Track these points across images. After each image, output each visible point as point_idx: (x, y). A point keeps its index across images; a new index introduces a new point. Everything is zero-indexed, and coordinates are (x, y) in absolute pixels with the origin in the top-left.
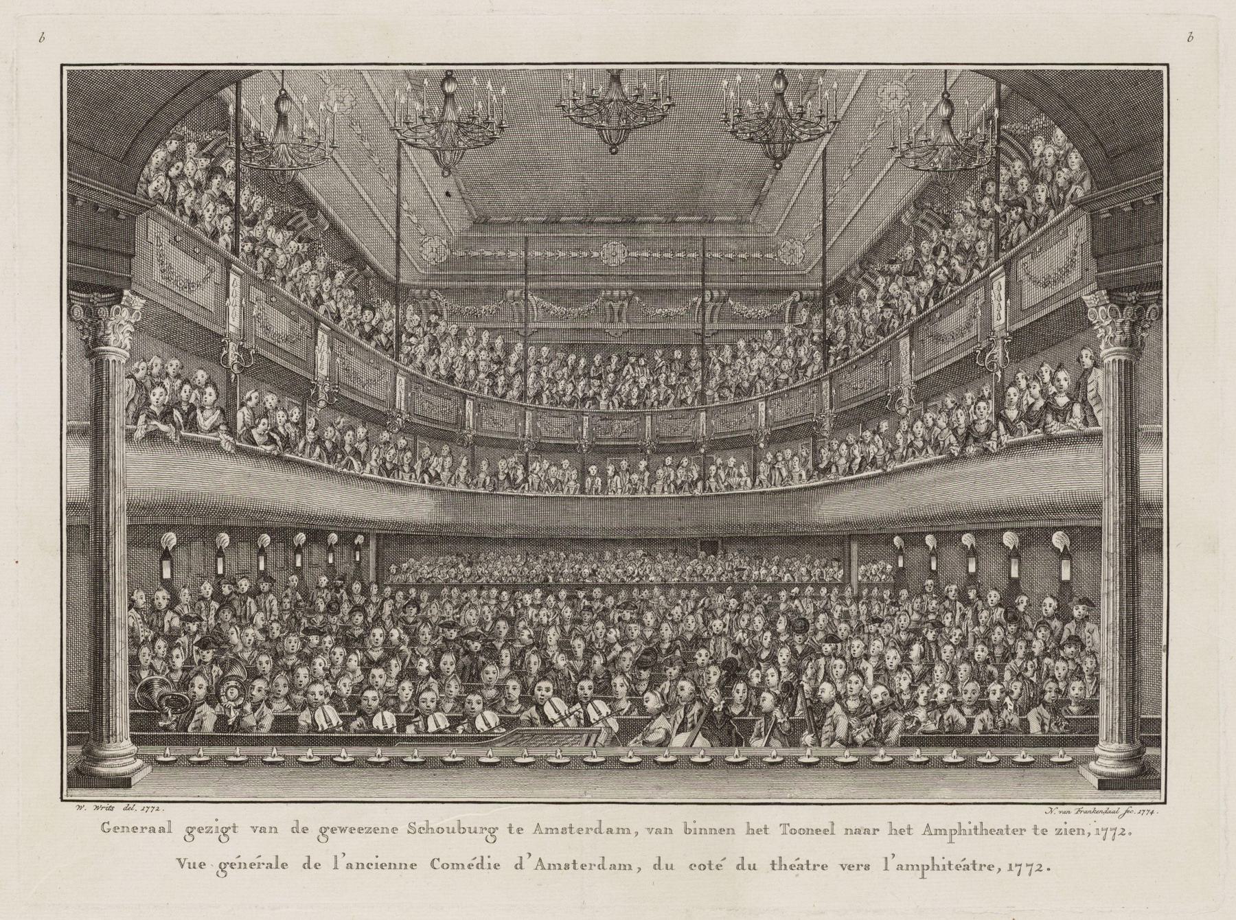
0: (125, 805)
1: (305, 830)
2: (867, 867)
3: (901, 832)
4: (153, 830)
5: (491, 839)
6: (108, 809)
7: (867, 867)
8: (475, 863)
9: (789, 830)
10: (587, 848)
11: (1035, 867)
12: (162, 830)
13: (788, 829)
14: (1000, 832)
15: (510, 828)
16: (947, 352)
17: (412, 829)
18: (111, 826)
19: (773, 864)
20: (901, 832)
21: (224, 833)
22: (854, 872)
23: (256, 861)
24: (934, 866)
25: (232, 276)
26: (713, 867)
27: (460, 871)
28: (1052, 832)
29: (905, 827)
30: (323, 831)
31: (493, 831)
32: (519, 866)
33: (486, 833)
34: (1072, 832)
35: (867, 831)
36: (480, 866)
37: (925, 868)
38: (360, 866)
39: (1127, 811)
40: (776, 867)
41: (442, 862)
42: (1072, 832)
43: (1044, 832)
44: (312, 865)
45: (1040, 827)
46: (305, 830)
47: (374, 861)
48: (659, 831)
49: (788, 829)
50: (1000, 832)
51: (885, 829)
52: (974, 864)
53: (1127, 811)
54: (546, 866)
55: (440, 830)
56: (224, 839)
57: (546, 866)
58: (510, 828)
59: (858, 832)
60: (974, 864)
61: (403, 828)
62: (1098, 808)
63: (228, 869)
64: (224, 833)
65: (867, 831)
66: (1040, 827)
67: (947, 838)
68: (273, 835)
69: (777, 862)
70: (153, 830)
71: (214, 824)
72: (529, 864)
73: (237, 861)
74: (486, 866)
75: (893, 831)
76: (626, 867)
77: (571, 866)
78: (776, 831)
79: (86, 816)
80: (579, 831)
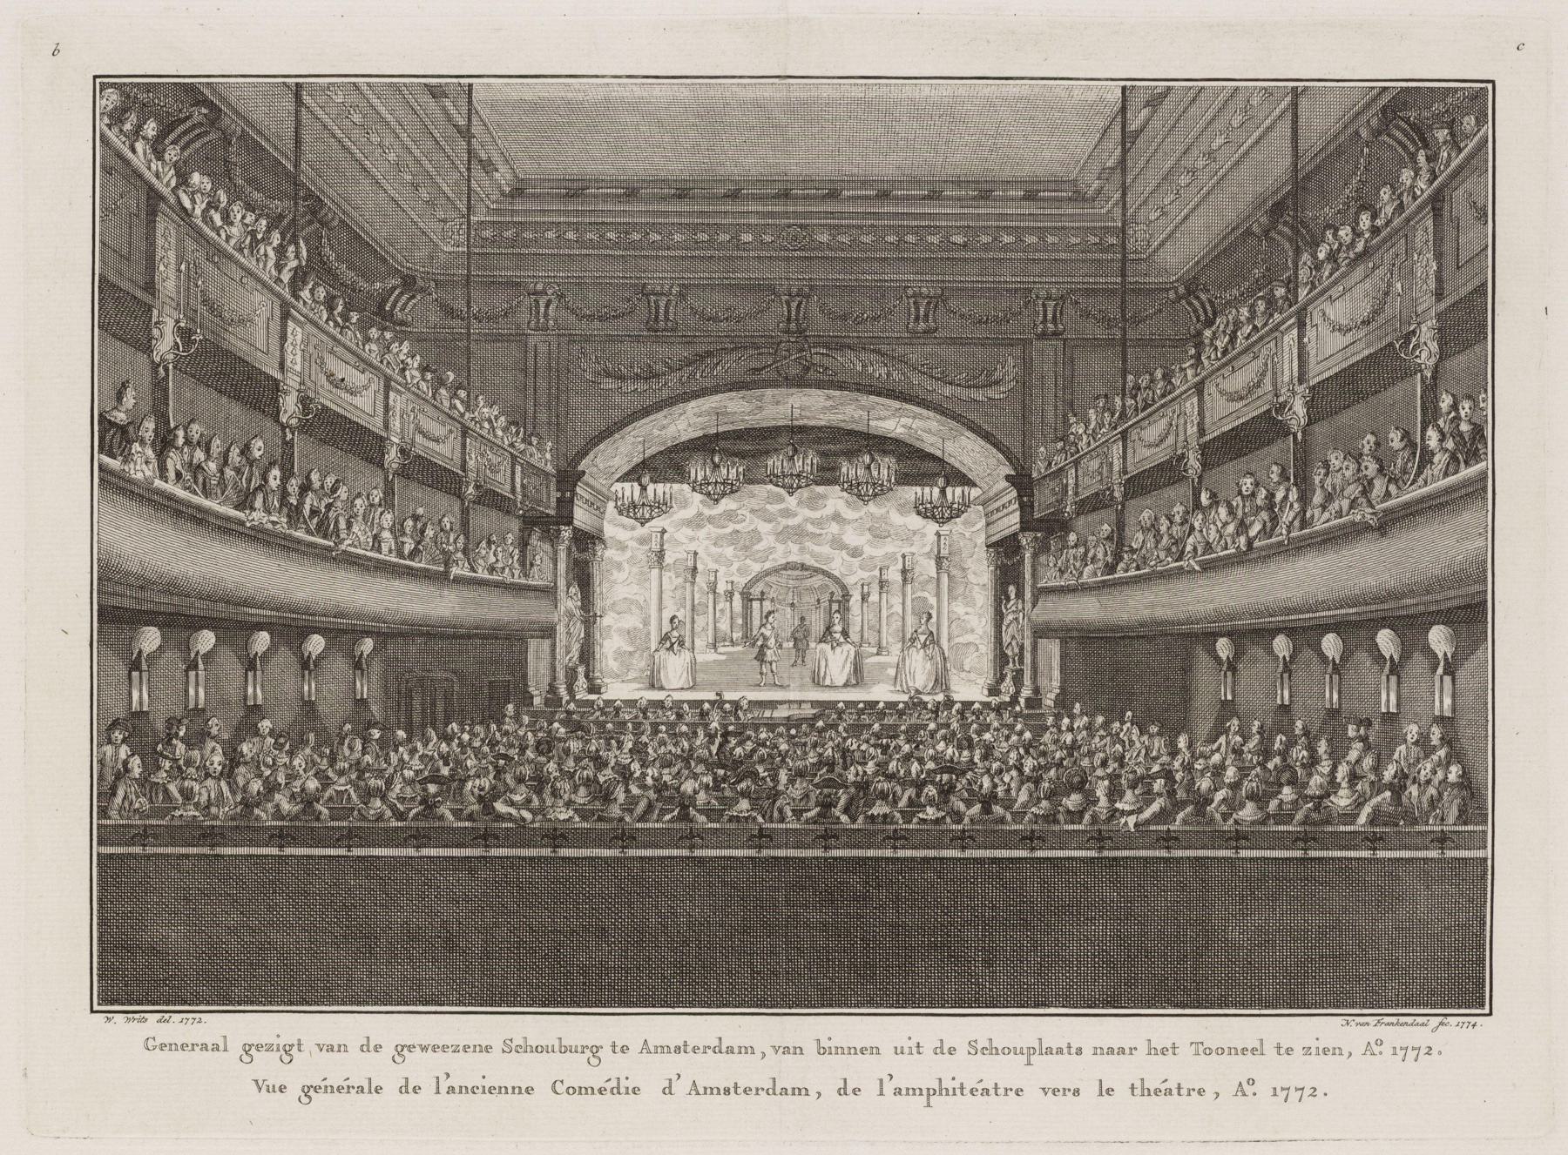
0: (159, 1016)
1: (377, 1048)
3: (1164, 1051)
4: (205, 1047)
5: (594, 1061)
6: (140, 1021)
8: (609, 1086)
9: (1202, 1049)
10: (751, 1071)
11: (1308, 1091)
12: (216, 1048)
13: (1201, 1048)
14: (1060, 1051)
15: (614, 1046)
18: (157, 1043)
19: (1133, 1087)
20: (1164, 1051)
21: (288, 1052)
23: (345, 1084)
24: (941, 1091)
25: (160, 226)
26: (966, 1091)
27: (503, 1096)
28: (1298, 1051)
29: (1169, 1046)
31: (595, 1050)
32: (668, 1090)
33: (588, 1053)
34: (1325, 1051)
35: (1122, 1051)
36: (616, 1090)
37: (931, 1093)
38: (463, 1089)
39: (1441, 1024)
41: (566, 1085)
42: (1325, 1051)
43: (1289, 1051)
44: (849, 1091)
48: (331, 1049)
50: (1060, 1051)
51: (811, 1048)
53: (1441, 1024)
54: (701, 1091)
56: (398, 1059)
57: (701, 1091)
58: (614, 1046)
61: (498, 1046)
63: (312, 1093)
64: (288, 1052)
65: (1122, 1051)
68: (343, 1054)
69: (1138, 1084)
70: (205, 1047)
71: (276, 1041)
72: (681, 1087)
73: (323, 1084)
74: (623, 1090)
76: (799, 1091)
77: (992, 1092)
78: (1185, 1050)
79: (129, 1032)
80: (695, 1050)
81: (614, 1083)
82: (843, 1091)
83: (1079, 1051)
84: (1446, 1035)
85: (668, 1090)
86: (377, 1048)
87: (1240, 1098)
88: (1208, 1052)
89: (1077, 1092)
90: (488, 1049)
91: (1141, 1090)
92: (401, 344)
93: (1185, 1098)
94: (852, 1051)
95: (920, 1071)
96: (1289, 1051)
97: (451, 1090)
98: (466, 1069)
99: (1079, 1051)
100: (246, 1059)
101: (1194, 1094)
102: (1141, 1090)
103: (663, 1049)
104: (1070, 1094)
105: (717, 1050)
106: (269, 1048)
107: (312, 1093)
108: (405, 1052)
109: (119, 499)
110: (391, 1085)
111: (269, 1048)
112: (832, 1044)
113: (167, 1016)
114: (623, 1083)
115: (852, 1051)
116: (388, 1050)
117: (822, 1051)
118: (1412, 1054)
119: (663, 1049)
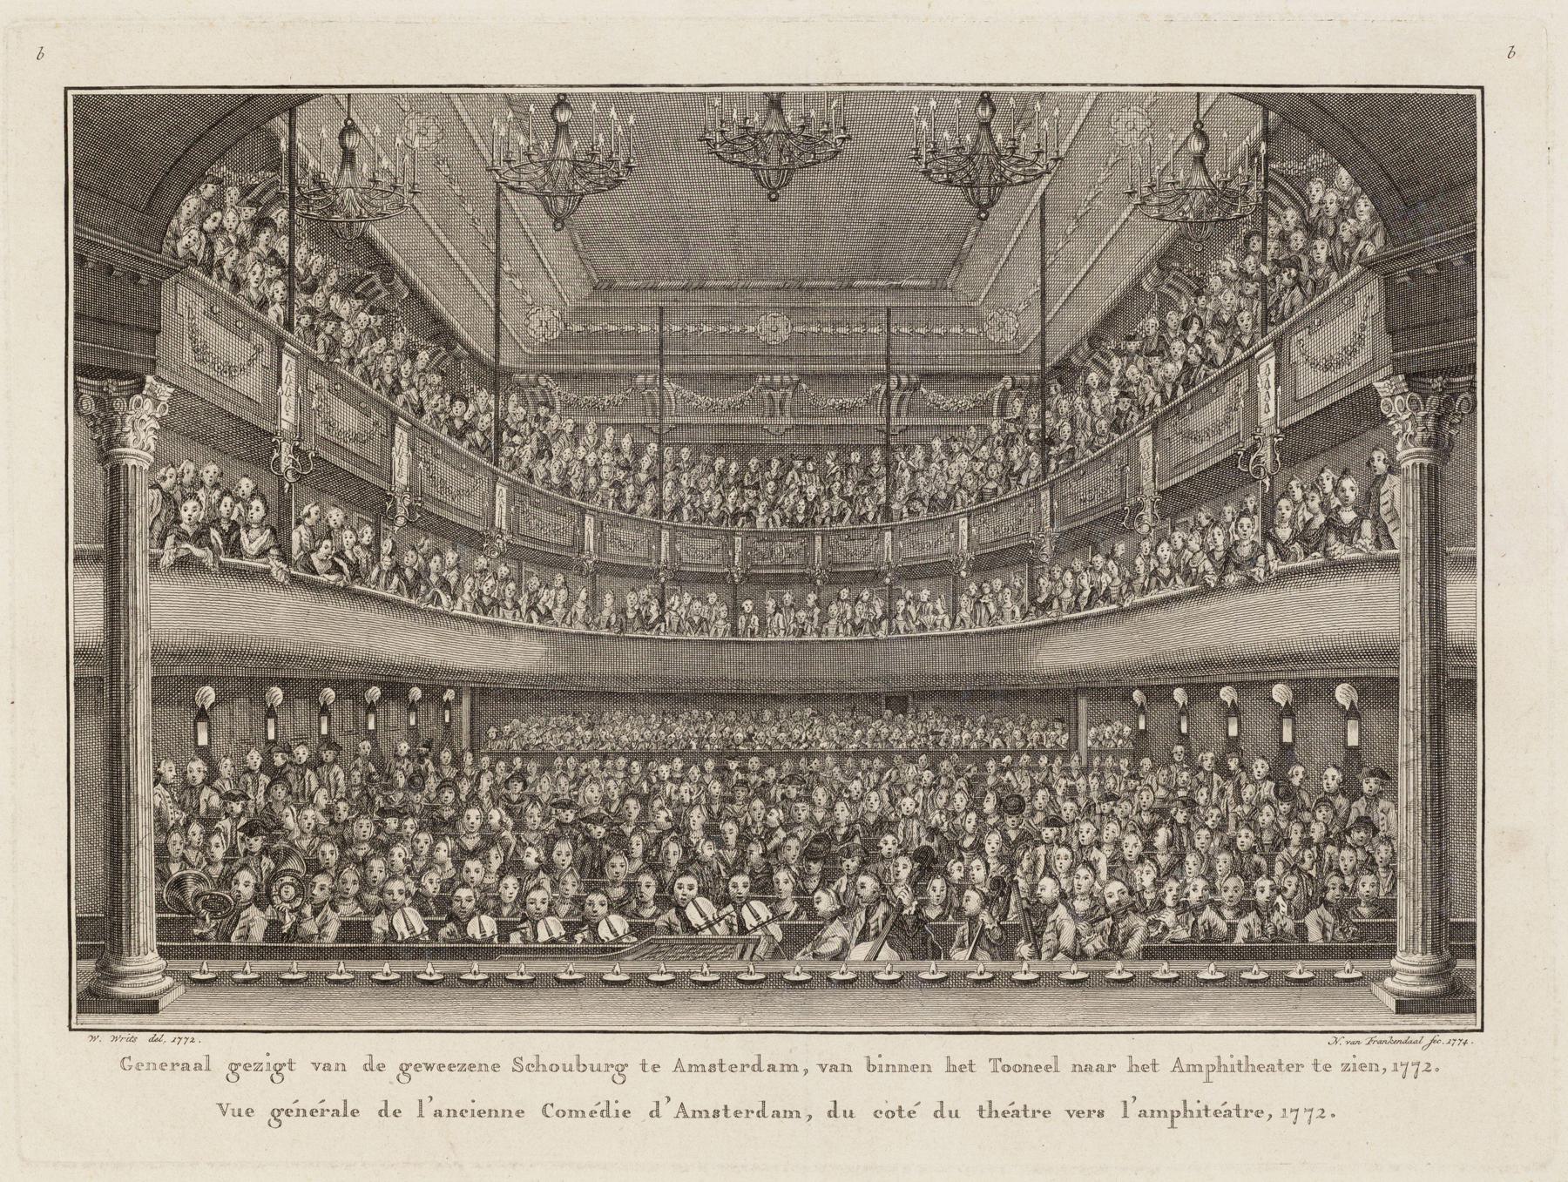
0: (151, 1035)
1: (381, 1067)
2: (1101, 1114)
3: (1144, 1068)
4: (186, 1067)
5: (619, 1079)
11: (1316, 1113)
12: (198, 1067)
13: (999, 1065)
14: (1271, 1068)
17: (518, 1065)
19: (981, 1110)
20: (1144, 1068)
23: (319, 1107)
26: (904, 1114)
28: (1337, 1069)
29: (1149, 1062)
32: (654, 1114)
33: (612, 1071)
35: (1100, 1068)
36: (605, 1113)
38: (452, 1113)
39: (1433, 1041)
40: (985, 1114)
44: (390, 1113)
47: (470, 1106)
48: (834, 1068)
49: (999, 1065)
50: (1271, 1068)
53: (1433, 1041)
60: (726, 1109)
63: (283, 1117)
65: (1100, 1068)
69: (986, 1107)
71: (265, 1060)
72: (668, 1110)
73: (294, 1107)
74: (612, 1113)
77: (722, 1113)
79: (105, 1048)
80: (732, 1068)
81: (603, 1106)
82: (383, 1113)
83: (1327, 1068)
84: (1448, 1052)
86: (381, 1067)
87: (681, 1119)
88: (1007, 1069)
89: (1101, 1114)
90: (495, 1067)
91: (988, 1111)
92: (681, 595)
93: (1030, 1120)
94: (903, 1068)
95: (1165, 1090)
96: (1327, 1068)
98: (453, 1090)
100: (233, 1077)
101: (1094, 1115)
102: (988, 1111)
103: (695, 1068)
104: (1094, 1115)
105: (757, 1068)
106: (258, 1067)
107: (283, 1117)
109: (1174, 659)
110: (369, 1110)
111: (258, 1067)
112: (883, 1061)
113: (159, 1035)
115: (903, 1068)
116: (392, 1070)
117: (871, 1068)
119: (695, 1068)
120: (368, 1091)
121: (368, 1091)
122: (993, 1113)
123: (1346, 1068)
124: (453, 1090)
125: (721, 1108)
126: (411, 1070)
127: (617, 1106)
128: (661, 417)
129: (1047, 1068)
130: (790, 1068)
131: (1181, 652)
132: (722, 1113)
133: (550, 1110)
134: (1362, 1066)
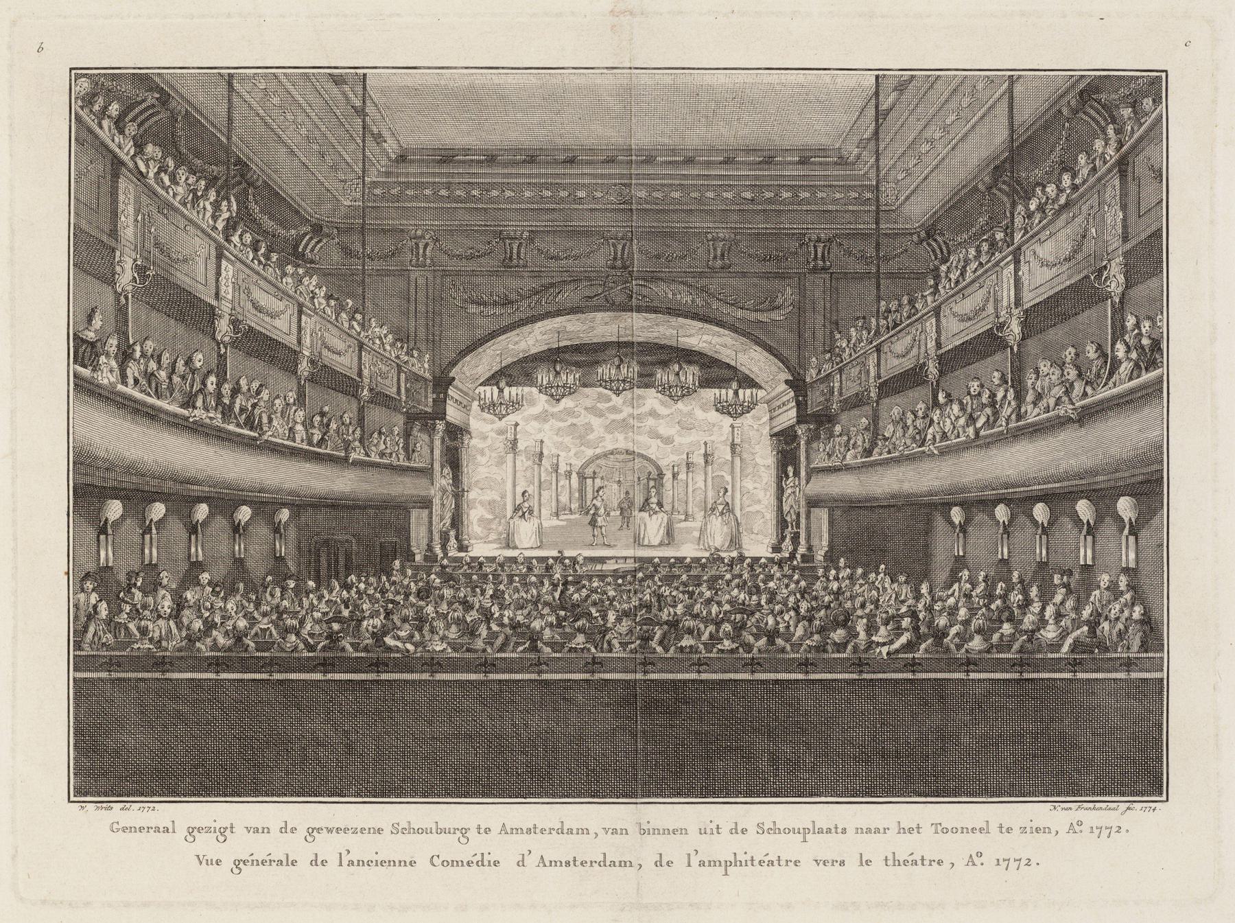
0: (122, 805)
1: (293, 830)
2: (842, 863)
3: (910, 830)
4: (157, 830)
5: (463, 840)
6: (106, 809)
7: (796, 863)
11: (1024, 862)
13: (939, 828)
16: (893, 365)
17: (396, 830)
19: (886, 860)
20: (910, 830)
22: (829, 867)
23: (268, 858)
24: (736, 863)
28: (1016, 831)
29: (914, 826)
30: (191, 831)
31: (464, 831)
32: (521, 863)
33: (458, 834)
36: (481, 863)
37: (728, 864)
38: (361, 863)
39: (1128, 808)
40: (890, 862)
41: (442, 859)
43: (1009, 830)
44: (664, 863)
45: (1005, 826)
46: (744, 831)
47: (374, 858)
49: (939, 828)
52: (923, 859)
53: (1128, 808)
55: (420, 831)
56: (309, 839)
59: (869, 831)
60: (923, 859)
62: (1098, 805)
63: (241, 865)
64: (223, 833)
65: (877, 831)
66: (1005, 826)
67: (800, 837)
69: (890, 857)
70: (157, 830)
71: (213, 825)
72: (532, 861)
73: (250, 859)
74: (486, 863)
75: (902, 830)
78: (927, 830)
81: (479, 857)
85: (521, 863)
87: (541, 868)
88: (945, 831)
89: (842, 863)
90: (379, 831)
93: (927, 867)
96: (1009, 830)
97: (351, 863)
98: (361, 847)
99: (844, 831)
107: (241, 865)
108: (315, 833)
112: (651, 826)
113: (128, 805)
114: (486, 857)
116: (302, 832)
118: (1105, 833)
120: (296, 846)
121: (296, 846)
122: (897, 863)
123: (858, 830)
124: (361, 847)
125: (571, 860)
126: (196, 832)
127: (350, 857)
128: (877, 223)
129: (981, 830)
130: (584, 831)
131: (997, 478)
132: (776, 863)
133: (435, 860)
134: (1038, 830)
